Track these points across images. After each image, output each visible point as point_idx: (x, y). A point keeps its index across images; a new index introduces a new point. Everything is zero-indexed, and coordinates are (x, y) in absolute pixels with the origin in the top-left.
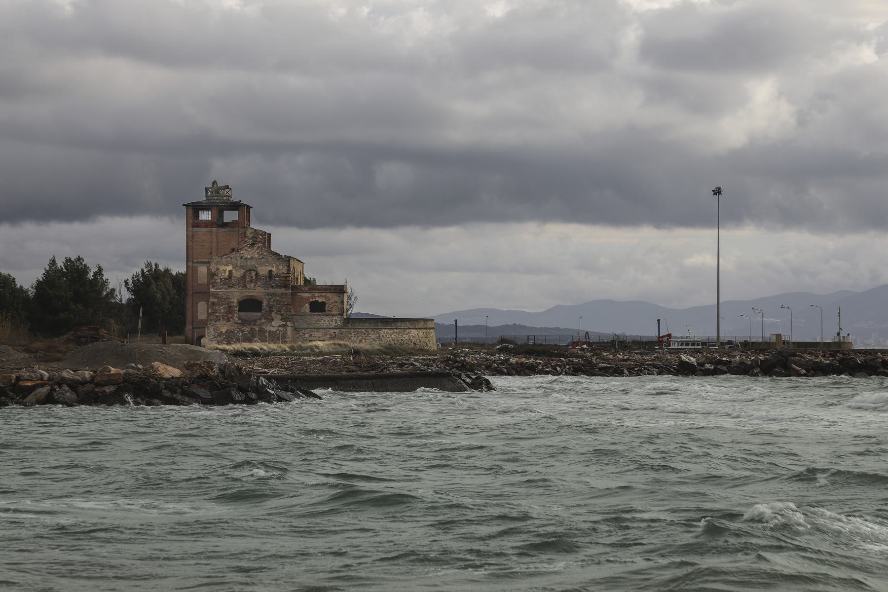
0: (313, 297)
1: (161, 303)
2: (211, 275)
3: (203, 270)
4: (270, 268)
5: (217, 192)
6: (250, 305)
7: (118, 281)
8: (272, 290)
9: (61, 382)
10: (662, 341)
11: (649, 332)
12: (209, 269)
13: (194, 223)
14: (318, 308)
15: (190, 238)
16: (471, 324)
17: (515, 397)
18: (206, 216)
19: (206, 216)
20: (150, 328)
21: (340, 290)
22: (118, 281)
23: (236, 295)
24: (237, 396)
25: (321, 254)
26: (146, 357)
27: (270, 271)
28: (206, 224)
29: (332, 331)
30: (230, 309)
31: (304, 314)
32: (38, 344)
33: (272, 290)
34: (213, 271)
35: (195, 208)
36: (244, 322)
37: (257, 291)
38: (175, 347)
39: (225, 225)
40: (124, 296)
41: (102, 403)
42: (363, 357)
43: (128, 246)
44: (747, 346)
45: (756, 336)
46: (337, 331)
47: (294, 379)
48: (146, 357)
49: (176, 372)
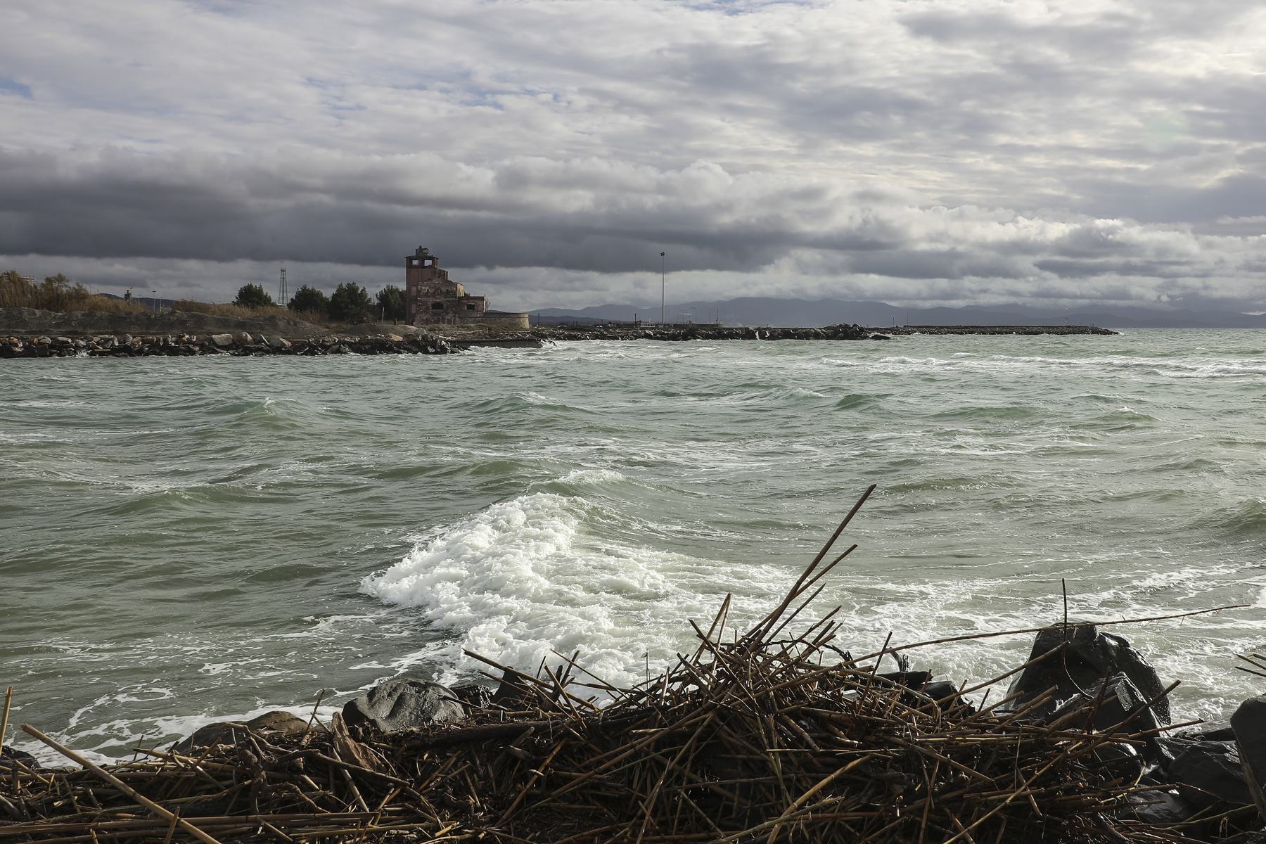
1: (393, 307)
2: (418, 291)
3: (414, 289)
6: (437, 306)
7: (373, 293)
9: (344, 343)
10: (637, 324)
11: (631, 320)
13: (409, 266)
14: (471, 307)
16: (683, 273)
17: (557, 351)
18: (415, 263)
19: (415, 263)
20: (388, 318)
21: (482, 299)
22: (373, 293)
23: (431, 301)
24: (431, 350)
25: (467, 283)
26: (385, 332)
30: (427, 308)
32: (333, 325)
35: (410, 259)
36: (435, 314)
37: (440, 299)
38: (400, 326)
40: (375, 301)
41: (766, 562)
43: (377, 281)
44: (676, 326)
45: (680, 322)
47: (459, 342)
48: (385, 332)
49: (401, 339)
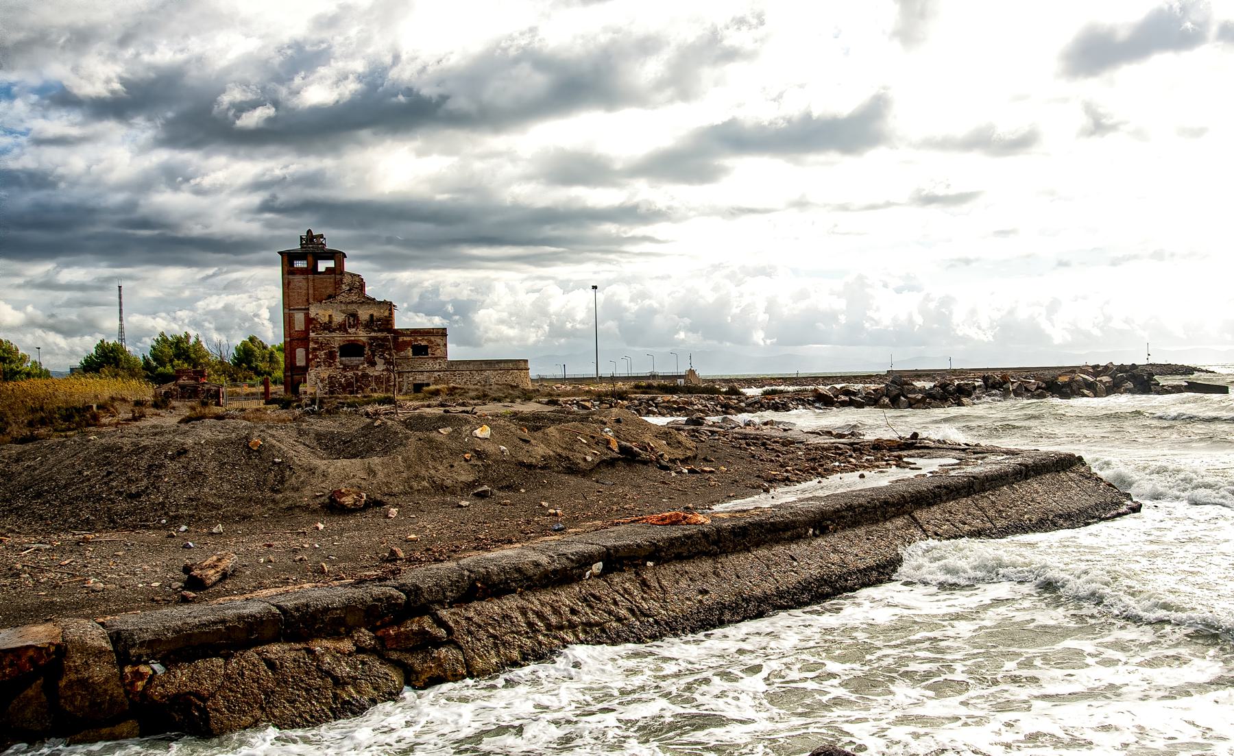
0: (416, 340)
4: (371, 312)
5: (311, 240)
8: (373, 334)
12: (307, 315)
13: (289, 271)
14: (420, 351)
15: (287, 286)
18: (300, 264)
19: (300, 264)
23: (338, 339)
27: (372, 316)
28: (301, 271)
29: (436, 374)
30: (331, 356)
31: (407, 358)
33: (373, 334)
34: (312, 316)
35: (288, 258)
37: (362, 335)
39: (213, 534)
42: (169, 367)
46: (441, 374)
